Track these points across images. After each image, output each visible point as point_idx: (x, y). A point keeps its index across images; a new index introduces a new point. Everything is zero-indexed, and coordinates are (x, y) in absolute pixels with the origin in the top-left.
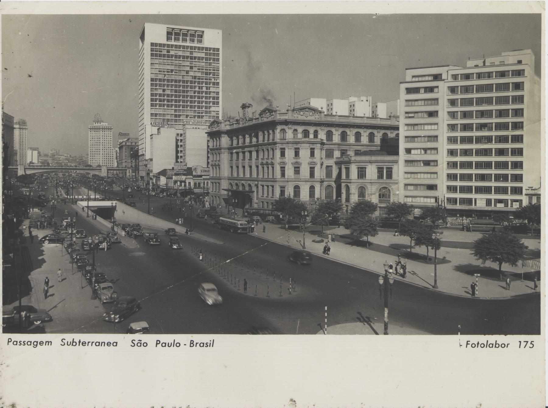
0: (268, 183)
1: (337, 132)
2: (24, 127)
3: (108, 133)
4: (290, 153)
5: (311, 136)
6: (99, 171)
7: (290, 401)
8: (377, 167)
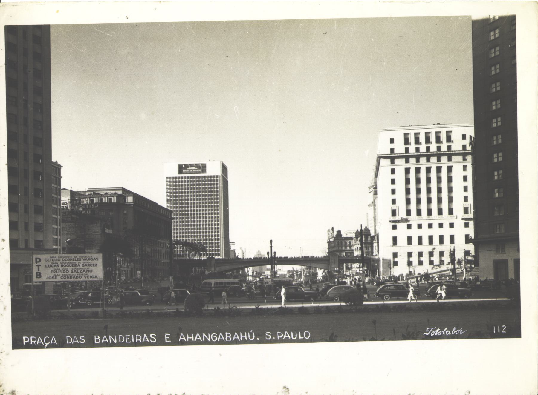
7: (283, 388)
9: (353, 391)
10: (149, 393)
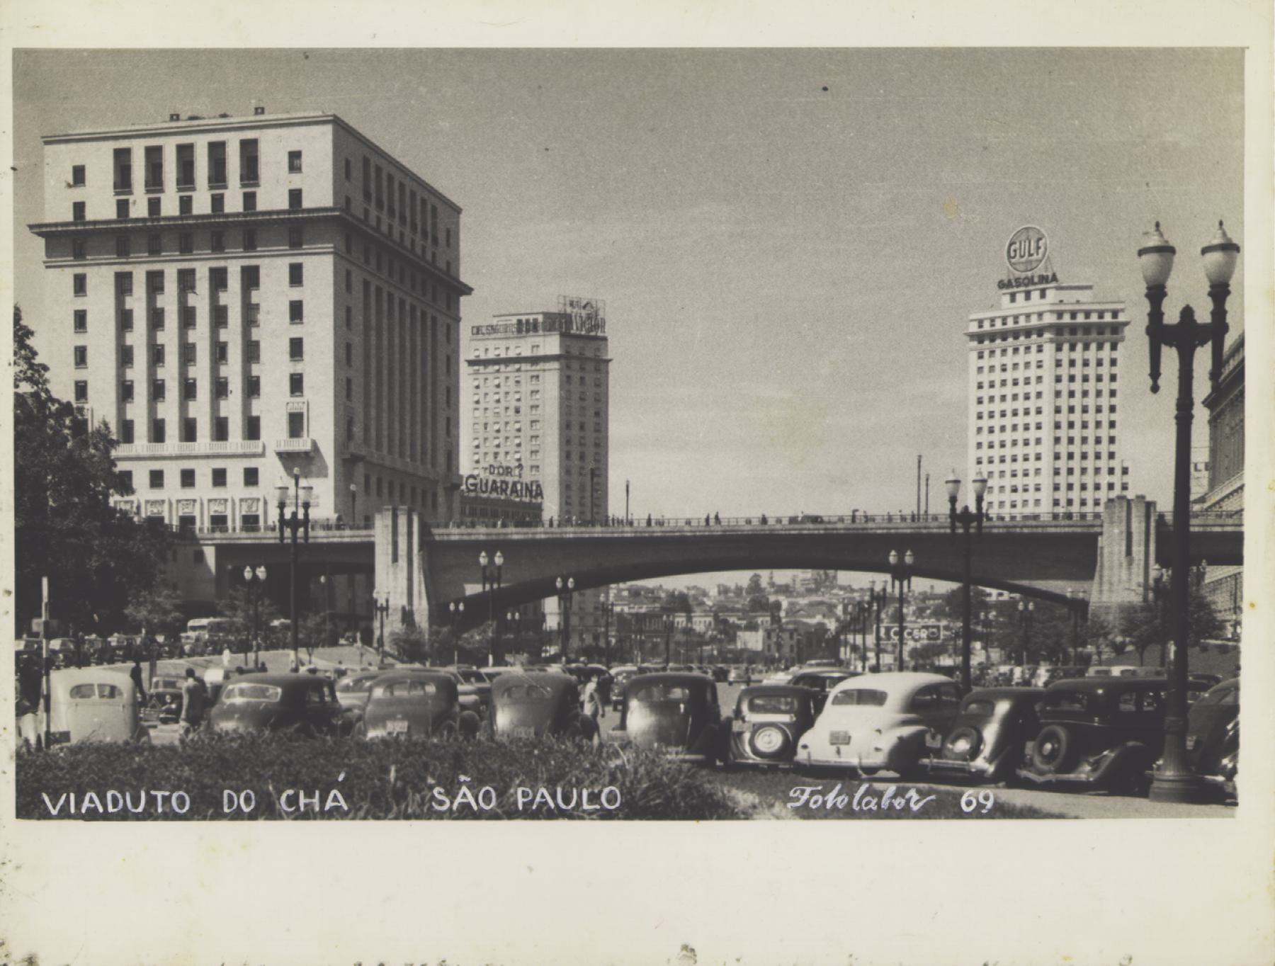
3: (1092, 354)
7: (682, 950)
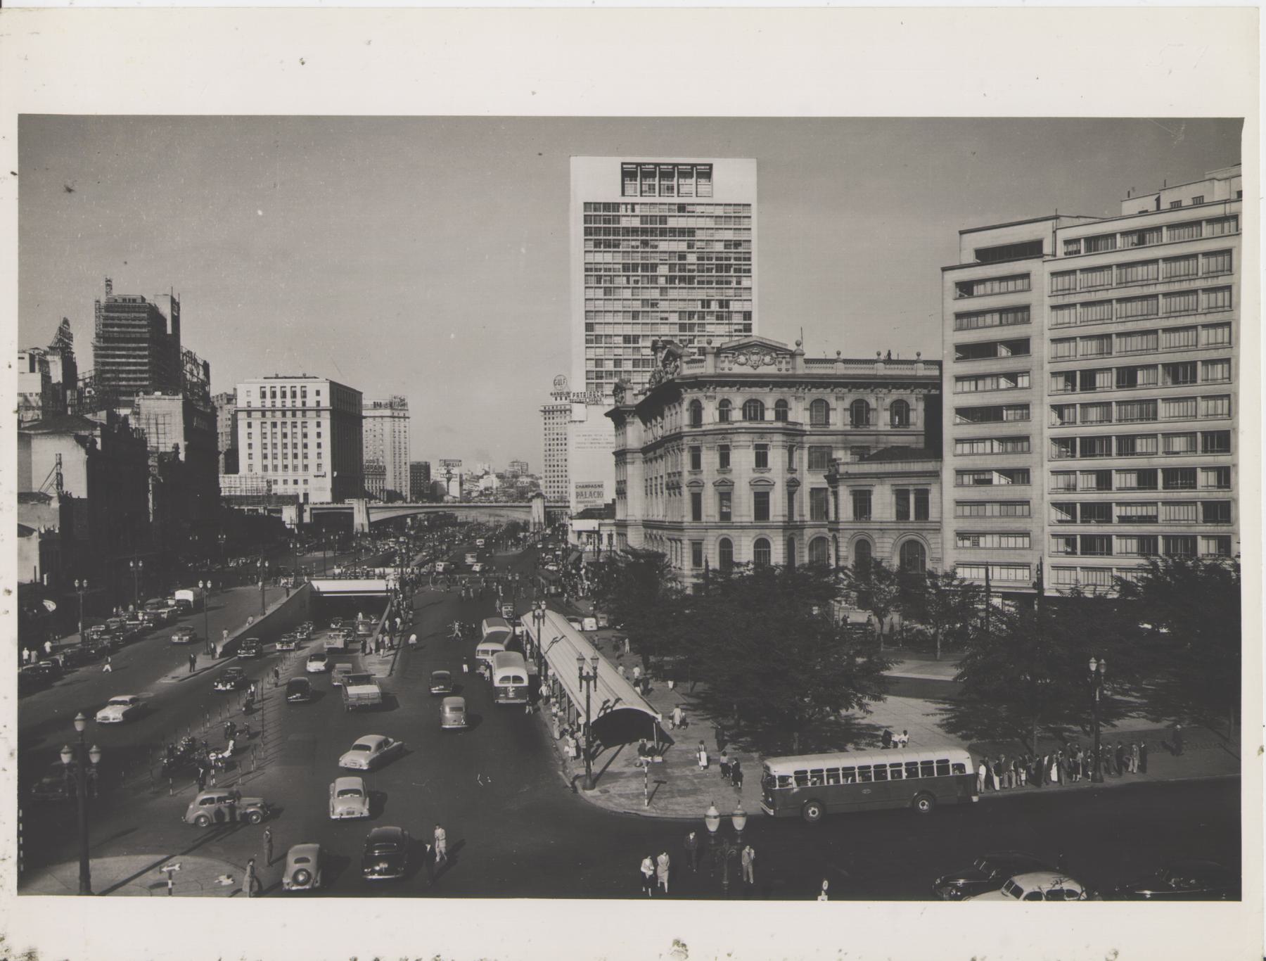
0: (672, 533)
1: (840, 403)
2: (401, 415)
4: (710, 459)
5: (770, 415)
6: (525, 509)
7: (673, 945)
8: (894, 488)
9: (840, 951)
10: (355, 955)
